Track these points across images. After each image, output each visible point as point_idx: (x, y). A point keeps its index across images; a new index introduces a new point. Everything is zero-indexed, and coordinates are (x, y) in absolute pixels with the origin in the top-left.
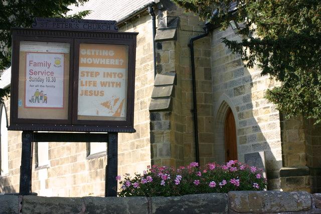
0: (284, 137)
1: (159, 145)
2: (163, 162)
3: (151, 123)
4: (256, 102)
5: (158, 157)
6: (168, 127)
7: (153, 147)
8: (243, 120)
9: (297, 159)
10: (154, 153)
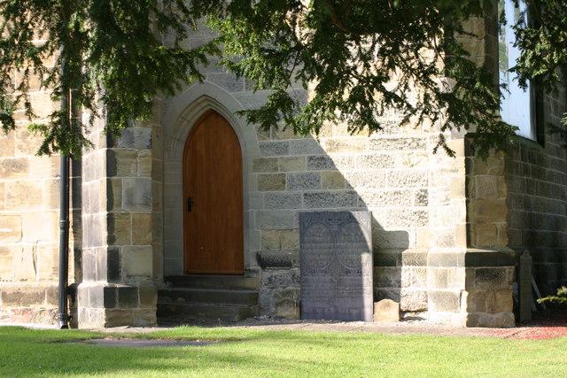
0: (471, 188)
1: (127, 181)
5: (124, 208)
6: (148, 143)
7: (113, 185)
8: (276, 141)
9: (493, 234)
10: (115, 198)
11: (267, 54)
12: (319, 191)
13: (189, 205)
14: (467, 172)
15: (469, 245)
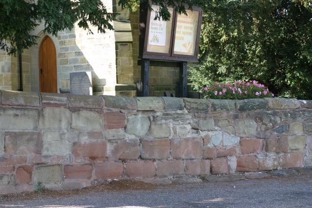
0: (118, 62)
2: (5, 78)
3: (116, 52)
4: (80, 34)
9: (127, 79)
11: (257, 93)
12: (78, 65)
13: (41, 71)
14: (117, 56)
15: (117, 83)
